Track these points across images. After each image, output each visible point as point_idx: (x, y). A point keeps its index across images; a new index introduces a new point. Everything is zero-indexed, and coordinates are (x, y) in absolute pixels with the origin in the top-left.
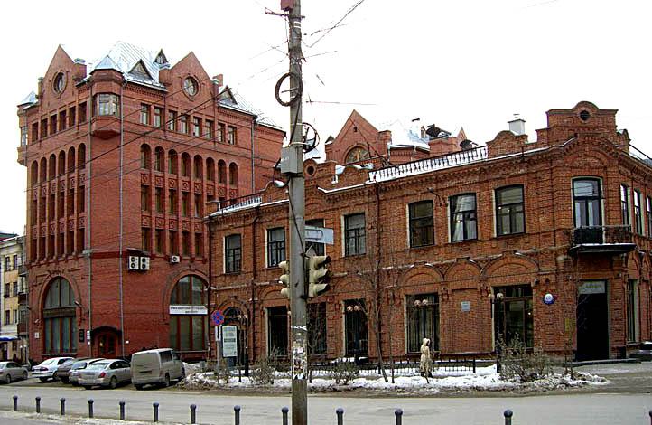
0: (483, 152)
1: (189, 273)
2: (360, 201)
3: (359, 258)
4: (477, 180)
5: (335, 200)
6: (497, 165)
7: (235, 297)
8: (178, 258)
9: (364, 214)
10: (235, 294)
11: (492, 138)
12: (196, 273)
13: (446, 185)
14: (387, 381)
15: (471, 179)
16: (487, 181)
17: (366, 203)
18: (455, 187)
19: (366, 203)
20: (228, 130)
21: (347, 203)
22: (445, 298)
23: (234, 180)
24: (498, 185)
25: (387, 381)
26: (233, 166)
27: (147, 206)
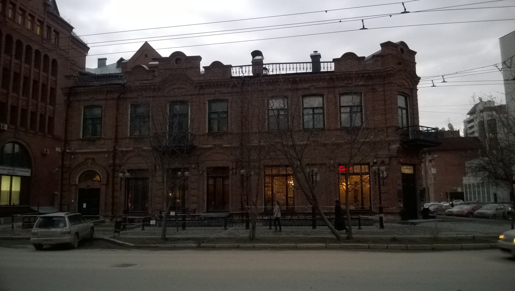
0: (309, 67)
1: (13, 140)
2: (225, 90)
3: (220, 135)
4: (105, 97)
5: (202, 87)
6: (152, 87)
7: (93, 159)
8: (6, 126)
9: (227, 100)
10: (92, 156)
11: (339, 56)
12: (20, 141)
13: (300, 86)
14: (495, 195)
15: (321, 84)
16: (203, 94)
17: (230, 93)
18: (308, 89)
19: (230, 93)
20: (53, 33)
21: (213, 91)
22: (234, 171)
23: (54, 73)
24: (211, 98)
25: (495, 195)
26: (54, 61)
27: (5, 85)
